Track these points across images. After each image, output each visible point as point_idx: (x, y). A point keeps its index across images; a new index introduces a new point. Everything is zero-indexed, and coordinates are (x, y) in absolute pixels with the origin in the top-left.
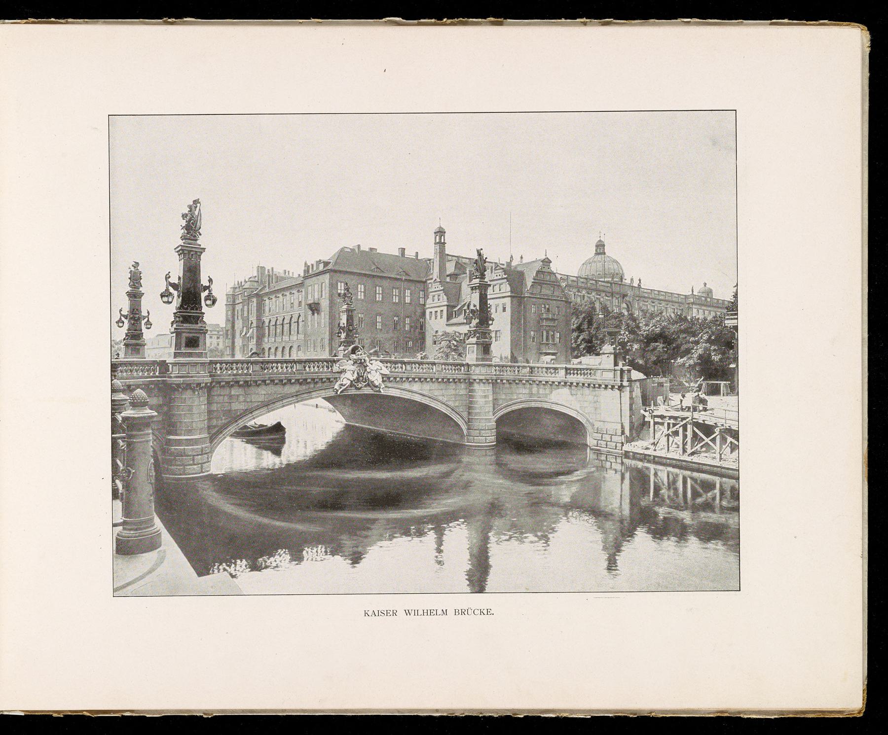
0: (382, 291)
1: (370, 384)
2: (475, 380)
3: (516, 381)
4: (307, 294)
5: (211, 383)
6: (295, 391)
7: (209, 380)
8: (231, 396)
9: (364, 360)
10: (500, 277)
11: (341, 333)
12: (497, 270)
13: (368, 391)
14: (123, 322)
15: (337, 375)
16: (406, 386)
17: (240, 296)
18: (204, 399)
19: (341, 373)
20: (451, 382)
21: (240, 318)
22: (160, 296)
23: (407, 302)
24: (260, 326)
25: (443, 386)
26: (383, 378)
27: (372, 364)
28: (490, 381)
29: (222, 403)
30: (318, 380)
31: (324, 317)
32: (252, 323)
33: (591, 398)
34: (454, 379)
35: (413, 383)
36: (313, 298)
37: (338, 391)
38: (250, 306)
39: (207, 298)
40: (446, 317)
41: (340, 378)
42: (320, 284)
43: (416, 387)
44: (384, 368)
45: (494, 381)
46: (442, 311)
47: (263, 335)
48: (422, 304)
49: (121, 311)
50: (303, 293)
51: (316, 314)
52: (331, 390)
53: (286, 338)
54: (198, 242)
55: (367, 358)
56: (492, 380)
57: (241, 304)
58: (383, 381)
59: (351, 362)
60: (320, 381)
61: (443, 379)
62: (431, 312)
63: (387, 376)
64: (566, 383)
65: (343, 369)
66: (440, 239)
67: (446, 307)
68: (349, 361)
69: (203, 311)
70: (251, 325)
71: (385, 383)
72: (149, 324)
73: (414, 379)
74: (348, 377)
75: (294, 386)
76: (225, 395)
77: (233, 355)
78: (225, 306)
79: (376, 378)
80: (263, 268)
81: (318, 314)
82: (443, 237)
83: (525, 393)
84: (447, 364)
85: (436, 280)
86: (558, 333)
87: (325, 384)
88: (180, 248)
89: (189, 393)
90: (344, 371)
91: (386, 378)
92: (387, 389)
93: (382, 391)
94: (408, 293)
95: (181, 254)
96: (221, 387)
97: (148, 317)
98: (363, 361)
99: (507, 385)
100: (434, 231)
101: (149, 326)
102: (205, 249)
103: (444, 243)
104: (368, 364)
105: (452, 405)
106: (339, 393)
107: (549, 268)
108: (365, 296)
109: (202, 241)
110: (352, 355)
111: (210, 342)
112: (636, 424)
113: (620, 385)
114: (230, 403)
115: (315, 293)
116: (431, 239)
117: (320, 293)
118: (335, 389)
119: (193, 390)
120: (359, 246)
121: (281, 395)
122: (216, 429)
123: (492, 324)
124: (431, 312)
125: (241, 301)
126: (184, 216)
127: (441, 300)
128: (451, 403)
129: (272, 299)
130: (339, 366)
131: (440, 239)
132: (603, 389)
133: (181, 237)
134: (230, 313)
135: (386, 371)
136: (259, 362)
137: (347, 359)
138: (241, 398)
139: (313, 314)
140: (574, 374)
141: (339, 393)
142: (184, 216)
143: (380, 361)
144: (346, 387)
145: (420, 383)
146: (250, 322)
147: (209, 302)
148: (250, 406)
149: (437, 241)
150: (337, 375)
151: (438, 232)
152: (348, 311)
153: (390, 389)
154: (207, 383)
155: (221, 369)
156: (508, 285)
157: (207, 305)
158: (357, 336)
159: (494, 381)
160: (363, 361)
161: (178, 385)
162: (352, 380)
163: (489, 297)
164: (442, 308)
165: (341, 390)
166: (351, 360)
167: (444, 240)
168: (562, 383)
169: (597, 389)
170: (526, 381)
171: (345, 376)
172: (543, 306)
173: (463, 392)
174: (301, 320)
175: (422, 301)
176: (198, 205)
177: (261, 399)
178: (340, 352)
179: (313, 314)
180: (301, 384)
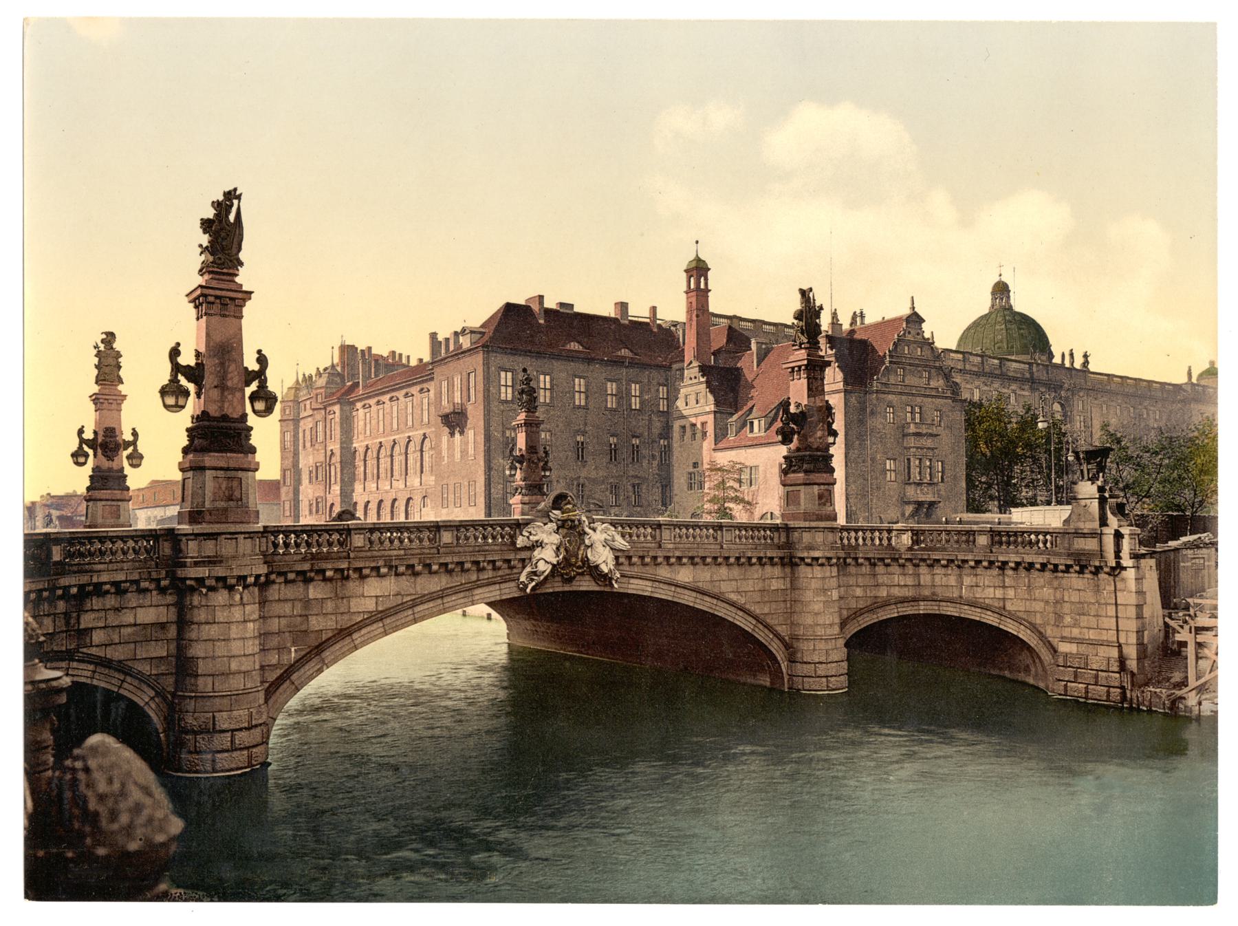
0: (587, 386)
1: (594, 571)
2: (802, 559)
3: (886, 561)
4: (439, 394)
5: (267, 575)
6: (439, 589)
7: (263, 570)
8: (307, 603)
9: (579, 520)
10: (696, 381)
11: (516, 469)
12: (692, 368)
13: (586, 584)
14: (87, 456)
15: (523, 555)
16: (664, 572)
17: (308, 402)
18: (252, 610)
19: (531, 548)
20: (754, 564)
21: (308, 444)
22: (159, 395)
23: (634, 407)
24: (348, 458)
25: (736, 572)
26: (617, 558)
27: (594, 530)
28: (834, 561)
29: (290, 616)
30: (485, 564)
31: (473, 436)
32: (332, 454)
33: (1047, 593)
34: (760, 559)
35: (677, 567)
36: (451, 404)
37: (526, 586)
38: (328, 421)
39: (254, 397)
40: (713, 436)
41: (530, 559)
42: (465, 374)
43: (685, 575)
44: (618, 538)
45: (841, 560)
46: (703, 424)
47: (353, 479)
48: (663, 412)
49: (83, 432)
50: (432, 393)
51: (457, 435)
52: (513, 584)
53: (384, 485)
54: (237, 279)
55: (584, 518)
56: (839, 558)
57: (310, 419)
58: (618, 564)
59: (553, 526)
60: (490, 567)
61: (738, 559)
62: (684, 427)
63: (626, 554)
64: (991, 563)
65: (537, 542)
66: (698, 283)
67: (712, 416)
68: (550, 525)
69: (249, 423)
70: (330, 458)
71: (621, 568)
72: (136, 459)
73: (679, 558)
74: (546, 558)
75: (435, 579)
76: (295, 600)
77: (297, 517)
78: (279, 423)
79: (603, 558)
80: (353, 348)
81: (462, 433)
82: (702, 279)
83: (905, 586)
84: (699, 527)
85: (691, 363)
86: (940, 463)
87: (500, 573)
88: (198, 292)
89: (221, 597)
90: (539, 544)
91: (620, 557)
92: (625, 580)
93: (616, 586)
94: (635, 389)
95: (201, 304)
96: (287, 582)
97: (134, 443)
98: (577, 522)
99: (866, 569)
100: (685, 268)
101: (135, 462)
102: (251, 293)
103: (707, 290)
104: (587, 530)
105: (758, 611)
106: (528, 590)
107: (918, 334)
108: (552, 398)
109: (244, 278)
110: (554, 511)
111: (442, 467)
112: (1149, 646)
113: (1114, 565)
114: (306, 616)
115: (456, 394)
116: (680, 282)
117: (465, 394)
118: (521, 582)
119: (231, 588)
120: (541, 298)
121: (413, 597)
122: (279, 672)
123: (834, 443)
124: (684, 427)
125: (311, 412)
126: (206, 225)
127: (702, 401)
128: (757, 610)
129: (370, 406)
130: (527, 534)
131: (698, 283)
132: (1077, 575)
133: (200, 271)
134: (288, 437)
135: (621, 543)
136: (365, 529)
137: (546, 520)
138: (329, 606)
139: (452, 434)
140: (1009, 543)
141: (528, 590)
142: (206, 225)
143: (611, 524)
144: (542, 578)
145: (692, 567)
146: (329, 453)
147: (260, 406)
148: (345, 622)
149: (692, 286)
150: (523, 555)
151: (691, 270)
152: (528, 424)
153: (632, 581)
154: (260, 575)
155: (286, 545)
156: (837, 369)
157: (254, 411)
158: (548, 473)
159: (841, 560)
160: (577, 522)
161: (200, 581)
162: (555, 563)
163: (827, 388)
164: (701, 419)
165: (534, 583)
166: (551, 521)
167: (706, 284)
168: (985, 564)
169: (1060, 574)
170: (907, 560)
171: (541, 556)
172: (909, 409)
173: (775, 585)
174: (398, 452)
175: (663, 406)
176: (235, 202)
177: (370, 605)
178: (513, 506)
179: (452, 434)
180: (450, 572)
